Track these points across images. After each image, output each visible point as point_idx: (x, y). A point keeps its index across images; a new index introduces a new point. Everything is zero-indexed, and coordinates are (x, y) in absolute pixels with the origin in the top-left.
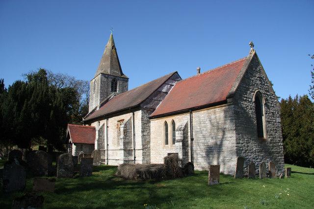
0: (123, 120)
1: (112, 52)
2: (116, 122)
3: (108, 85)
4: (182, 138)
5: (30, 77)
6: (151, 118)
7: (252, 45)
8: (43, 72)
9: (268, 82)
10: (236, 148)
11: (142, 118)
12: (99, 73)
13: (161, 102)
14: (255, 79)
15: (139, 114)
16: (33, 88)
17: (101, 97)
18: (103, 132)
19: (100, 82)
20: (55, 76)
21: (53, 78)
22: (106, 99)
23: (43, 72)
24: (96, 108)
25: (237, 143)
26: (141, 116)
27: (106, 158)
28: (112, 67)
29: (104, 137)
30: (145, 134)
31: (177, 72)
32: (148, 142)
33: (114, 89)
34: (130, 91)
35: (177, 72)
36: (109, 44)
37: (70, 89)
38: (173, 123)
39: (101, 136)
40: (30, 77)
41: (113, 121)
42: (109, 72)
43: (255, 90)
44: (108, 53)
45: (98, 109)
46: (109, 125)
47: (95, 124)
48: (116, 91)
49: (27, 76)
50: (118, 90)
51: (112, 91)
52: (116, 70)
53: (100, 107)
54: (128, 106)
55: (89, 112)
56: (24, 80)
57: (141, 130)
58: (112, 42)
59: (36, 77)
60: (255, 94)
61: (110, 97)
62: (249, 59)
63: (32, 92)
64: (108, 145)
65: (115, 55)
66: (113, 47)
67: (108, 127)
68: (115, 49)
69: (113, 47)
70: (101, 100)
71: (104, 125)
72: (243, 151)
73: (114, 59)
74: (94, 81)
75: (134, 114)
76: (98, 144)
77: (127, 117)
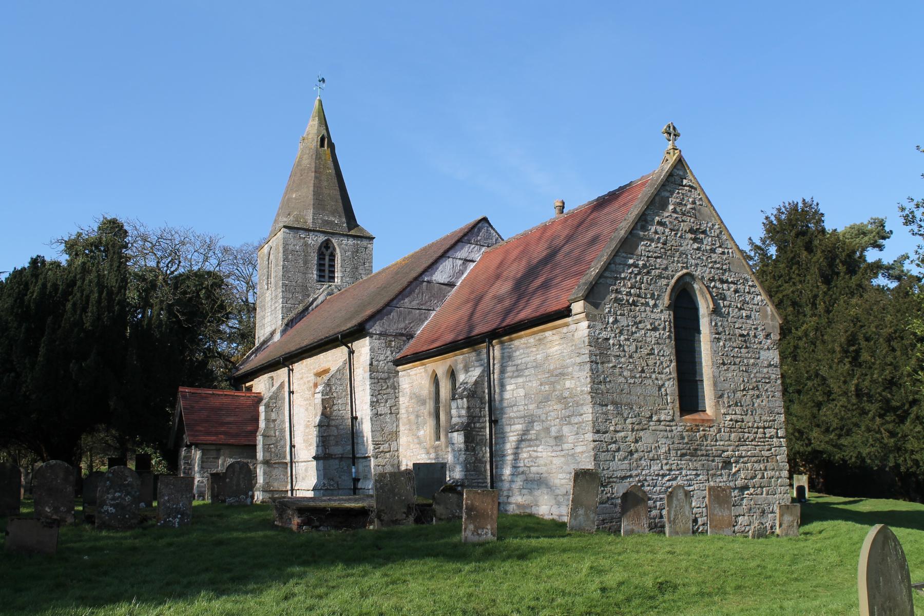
0: (329, 369)
1: (318, 157)
2: (312, 378)
3: (306, 262)
4: (465, 420)
5: (71, 247)
6: (398, 362)
7: (672, 132)
8: (114, 228)
9: (730, 244)
10: (592, 445)
11: (371, 364)
12: (282, 225)
13: (433, 313)
14: (292, 315)
15: (363, 348)
16: (73, 283)
17: (285, 300)
18: (280, 409)
19: (281, 255)
20: (154, 239)
21: (148, 245)
22: (301, 308)
23: (114, 228)
24: (272, 334)
25: (598, 432)
26: (368, 358)
27: (289, 487)
28: (319, 203)
29: (283, 422)
30: (382, 409)
31: (485, 220)
32: (391, 433)
33: (326, 272)
34: (379, 273)
35: (485, 220)
36: (312, 127)
37: (200, 276)
38: (452, 375)
39: (274, 421)
40: (71, 247)
41: (305, 370)
42: (309, 218)
43: (677, 271)
44: (309, 162)
45: (277, 337)
46: (295, 387)
47: (260, 385)
48: (332, 278)
49: (63, 247)
50: (338, 274)
51: (321, 278)
52: (333, 213)
53: (284, 332)
54: (337, 330)
55: (257, 344)
56: (57, 255)
57: (368, 398)
58: (320, 124)
59: (95, 245)
60: (673, 281)
61: (315, 300)
62: (657, 180)
63: (67, 293)
64: (292, 446)
65: (330, 163)
66: (322, 140)
67: (291, 392)
68: (332, 146)
69: (325, 141)
70: (286, 310)
71: (282, 386)
72: (621, 455)
73: (324, 177)
74: (266, 249)
75: (351, 352)
76: (264, 445)
77: (334, 358)
